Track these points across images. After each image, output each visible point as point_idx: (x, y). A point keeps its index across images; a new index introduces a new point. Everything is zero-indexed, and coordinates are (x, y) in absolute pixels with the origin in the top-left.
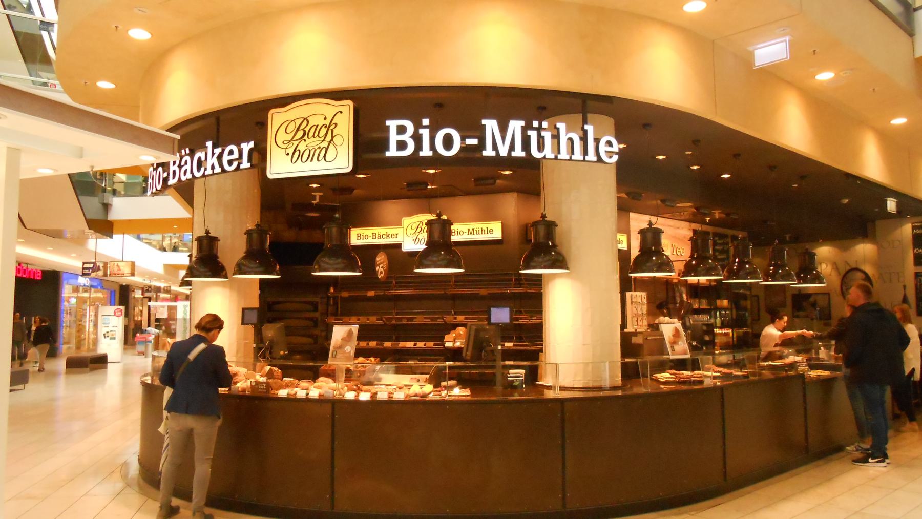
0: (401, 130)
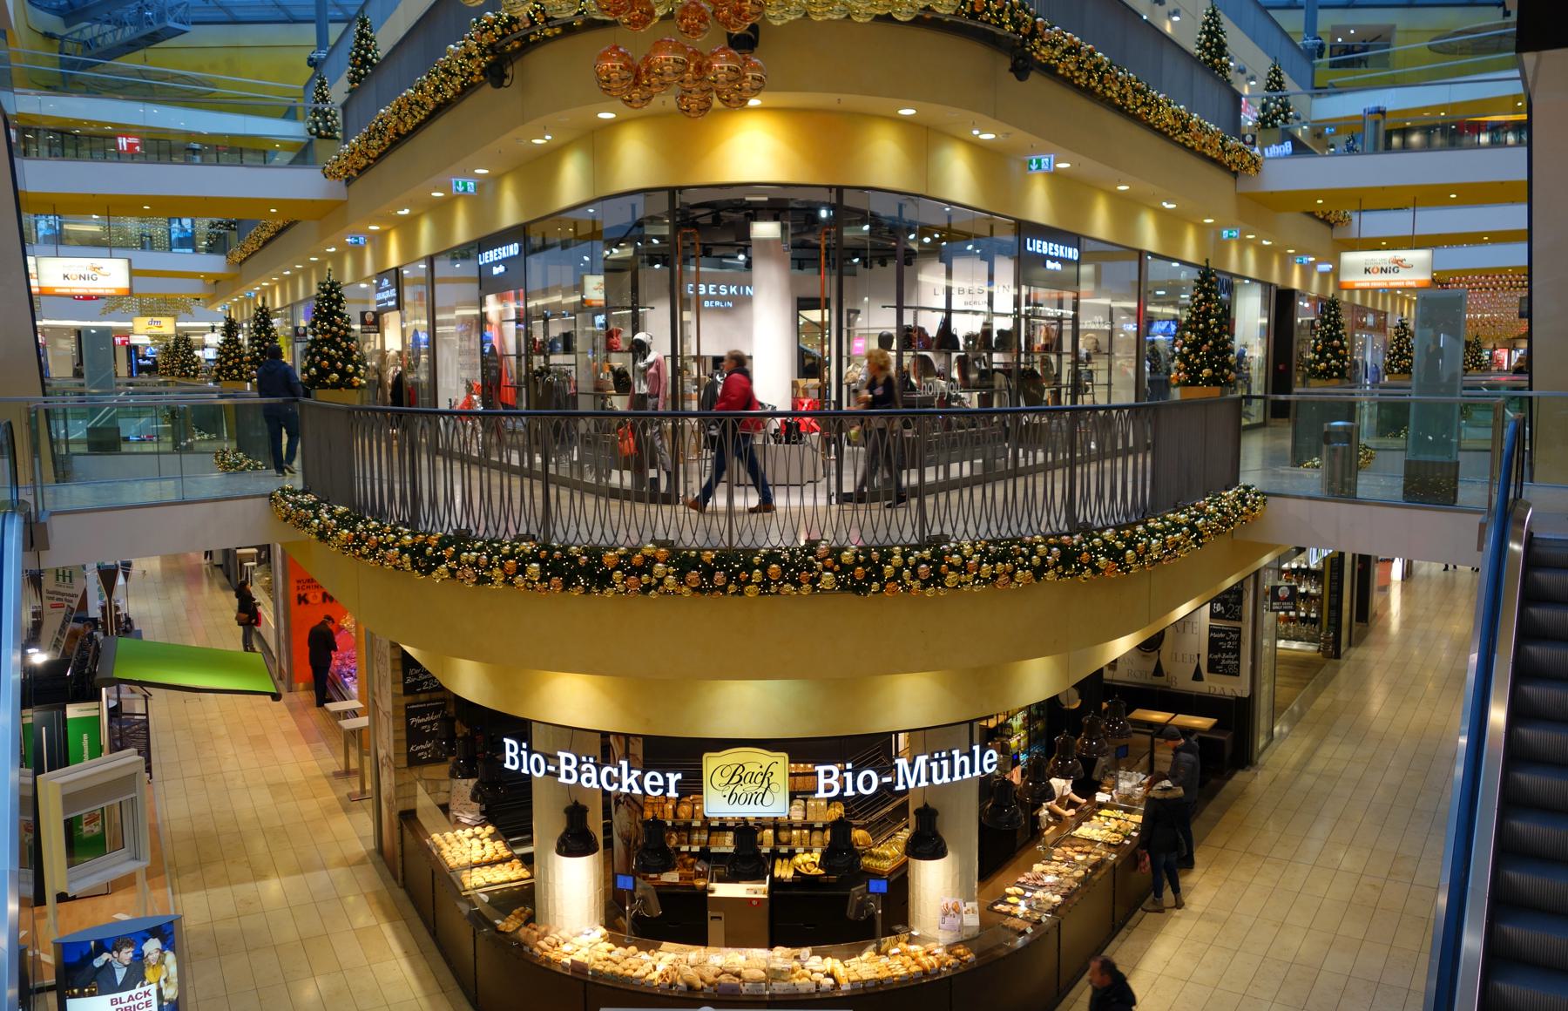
0: (829, 774)
